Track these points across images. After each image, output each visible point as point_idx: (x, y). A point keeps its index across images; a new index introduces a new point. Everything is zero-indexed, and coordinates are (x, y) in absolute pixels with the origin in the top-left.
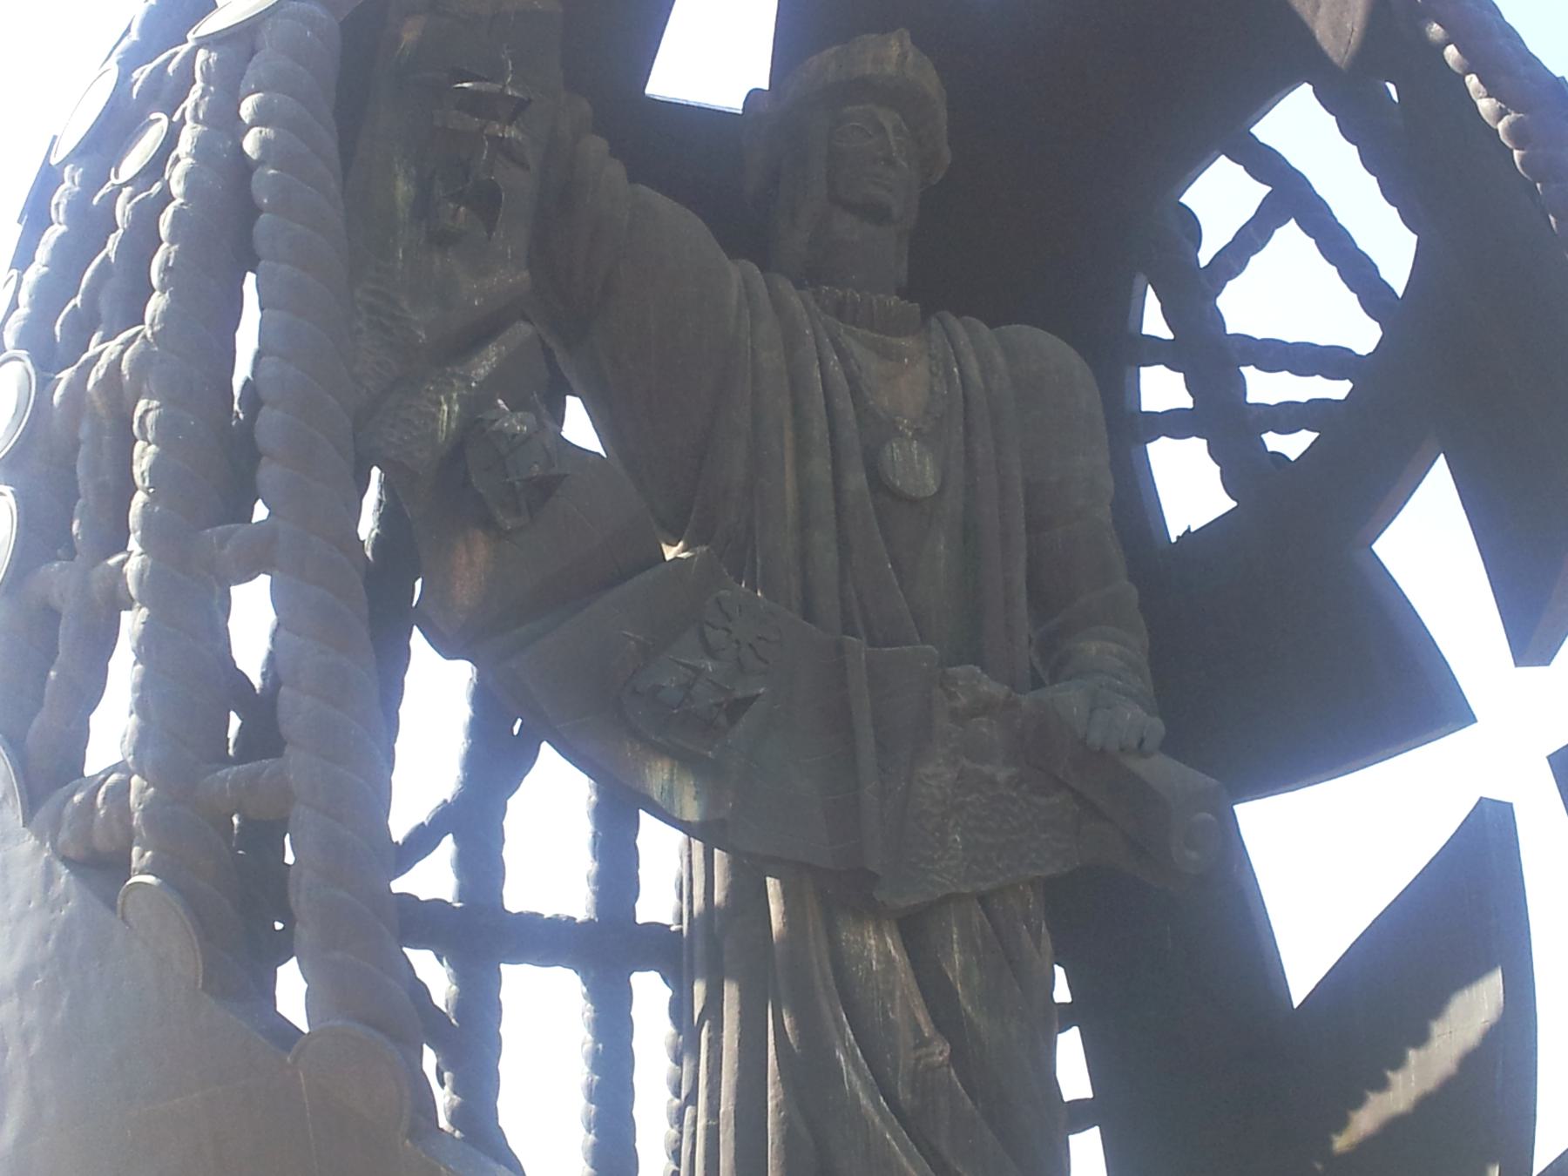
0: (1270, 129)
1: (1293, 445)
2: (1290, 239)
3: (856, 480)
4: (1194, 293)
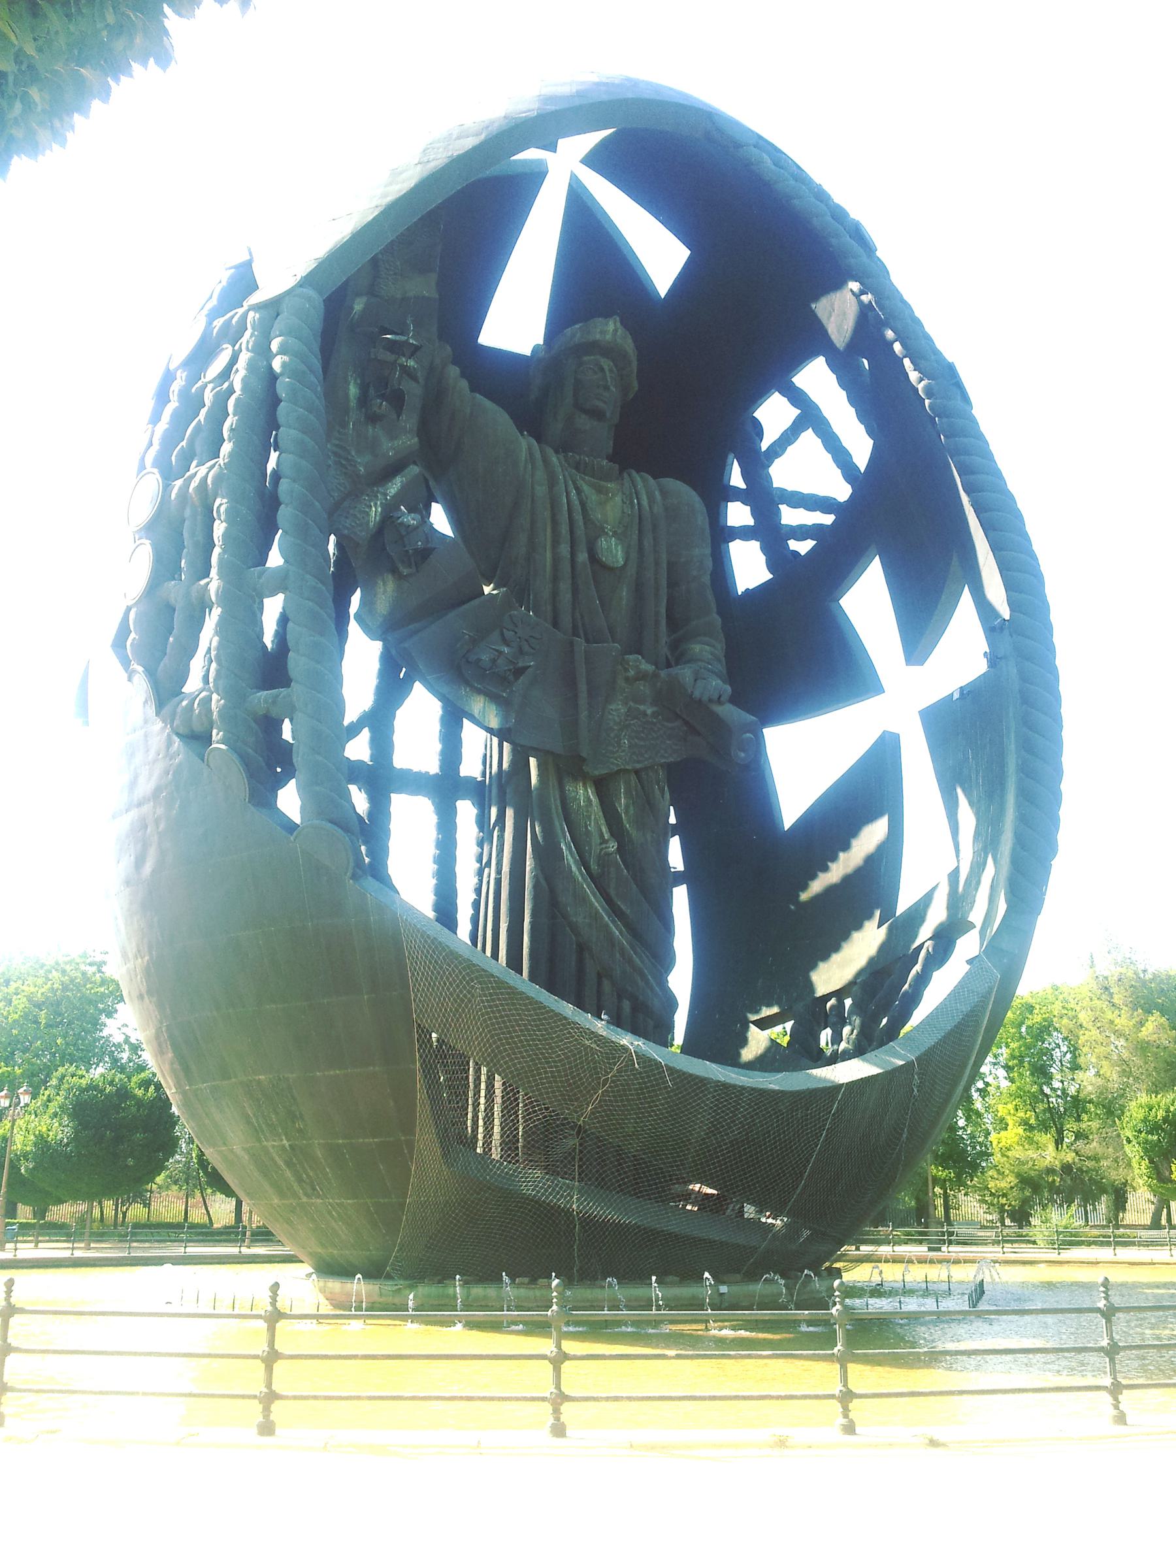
1: (803, 547)
3: (583, 557)
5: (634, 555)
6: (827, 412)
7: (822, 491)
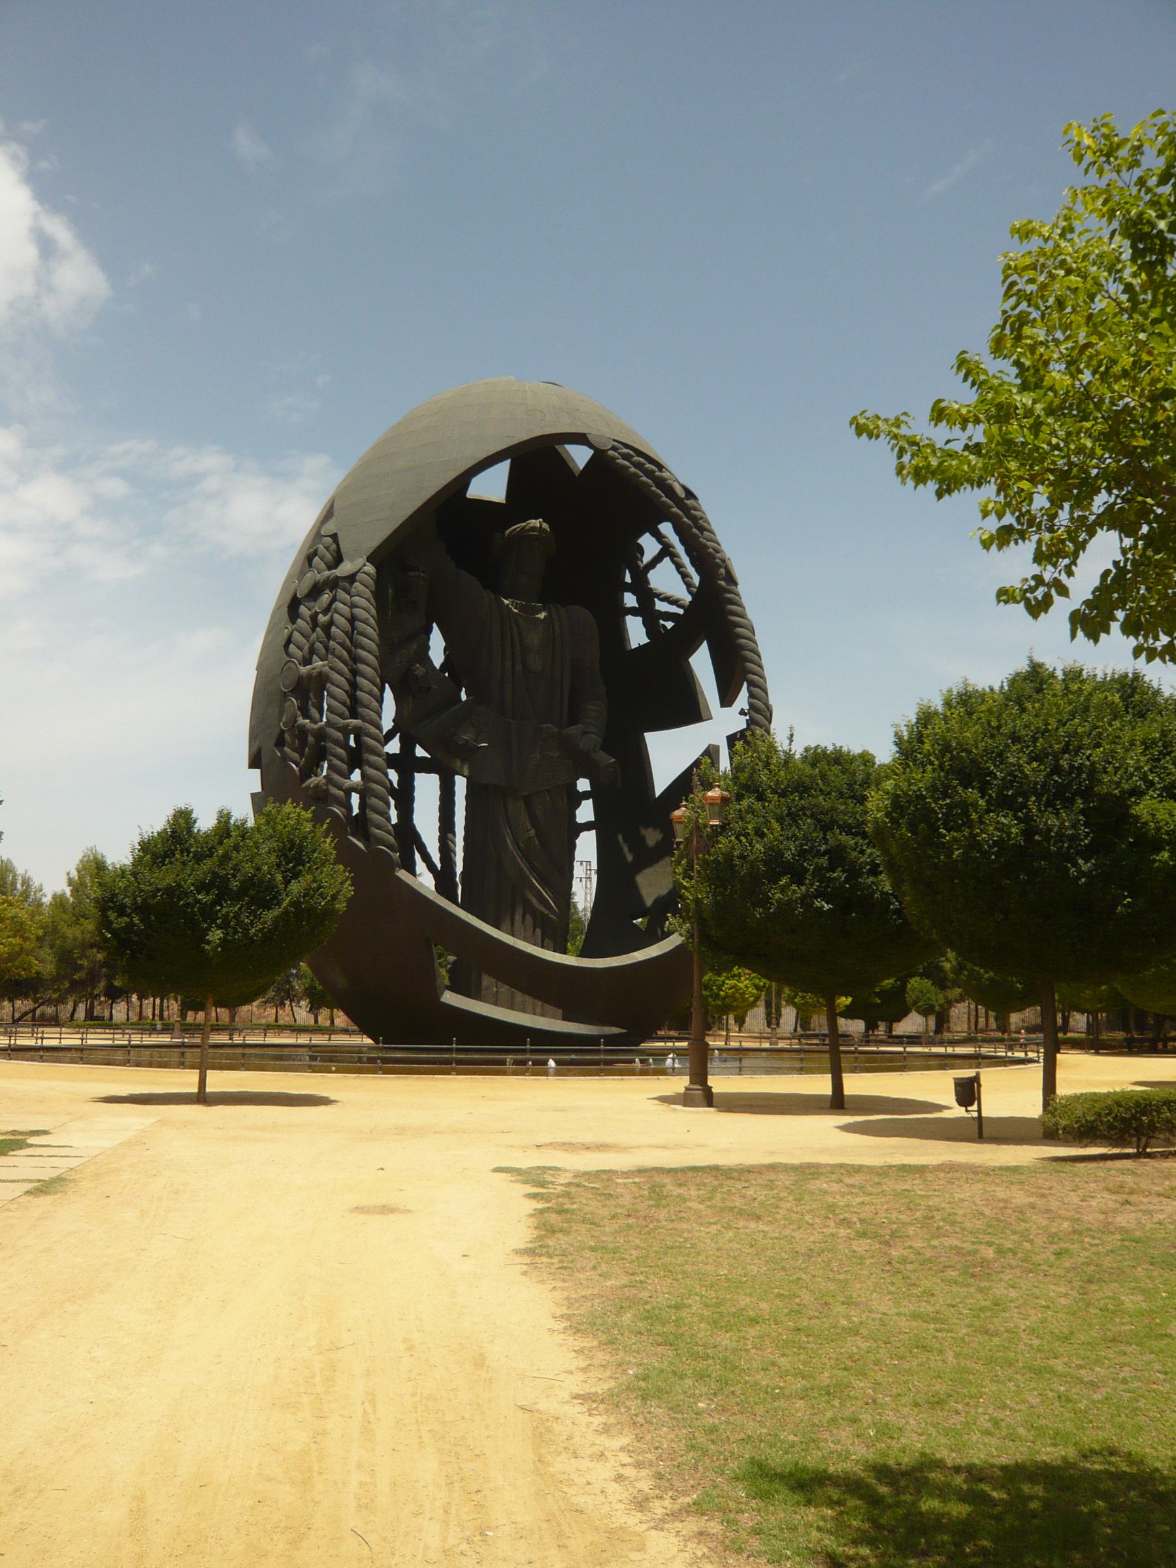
2: (667, 560)
3: (519, 667)
4: (641, 576)
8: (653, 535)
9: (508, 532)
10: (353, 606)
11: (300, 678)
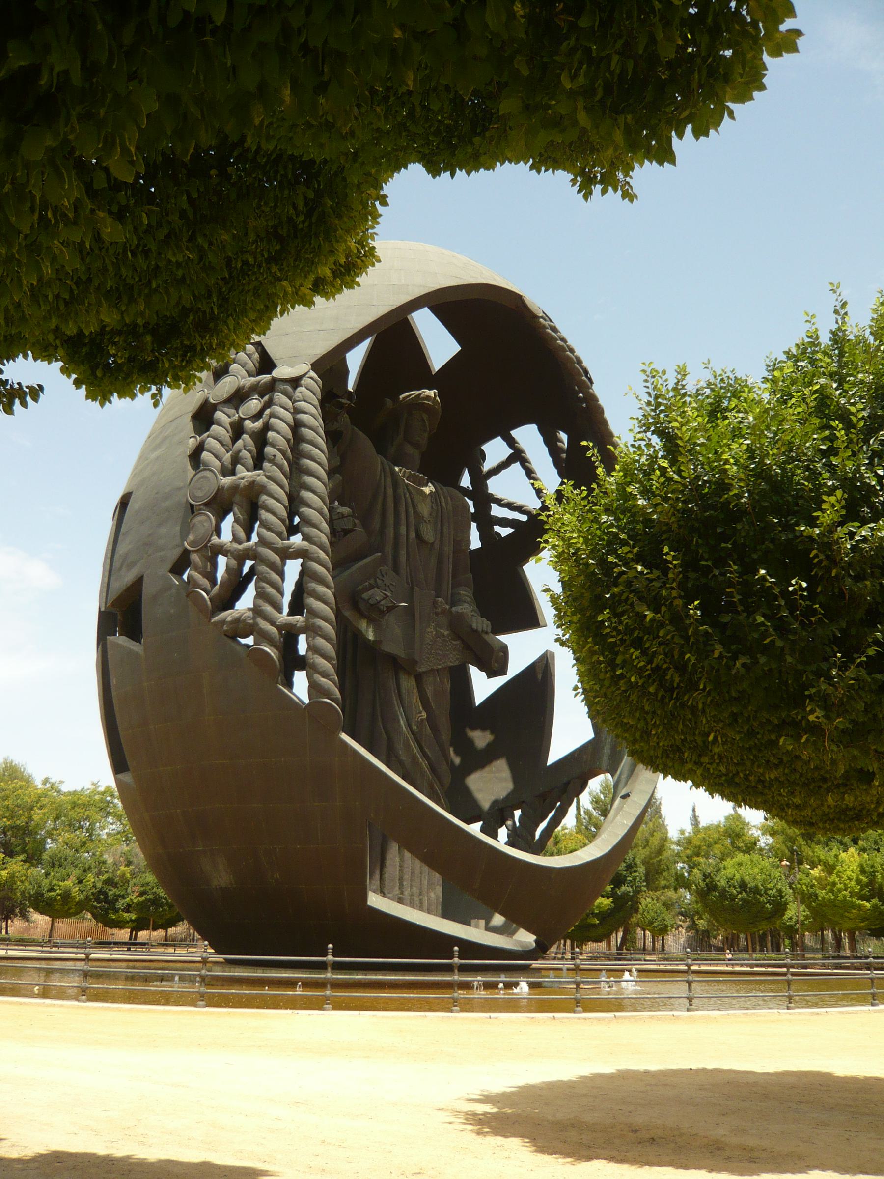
0: (515, 433)
1: (505, 532)
2: (516, 467)
3: (413, 534)
5: (439, 536)
6: (529, 455)
7: (519, 501)
8: (504, 439)
9: (401, 397)
10: (297, 411)
11: (220, 490)
